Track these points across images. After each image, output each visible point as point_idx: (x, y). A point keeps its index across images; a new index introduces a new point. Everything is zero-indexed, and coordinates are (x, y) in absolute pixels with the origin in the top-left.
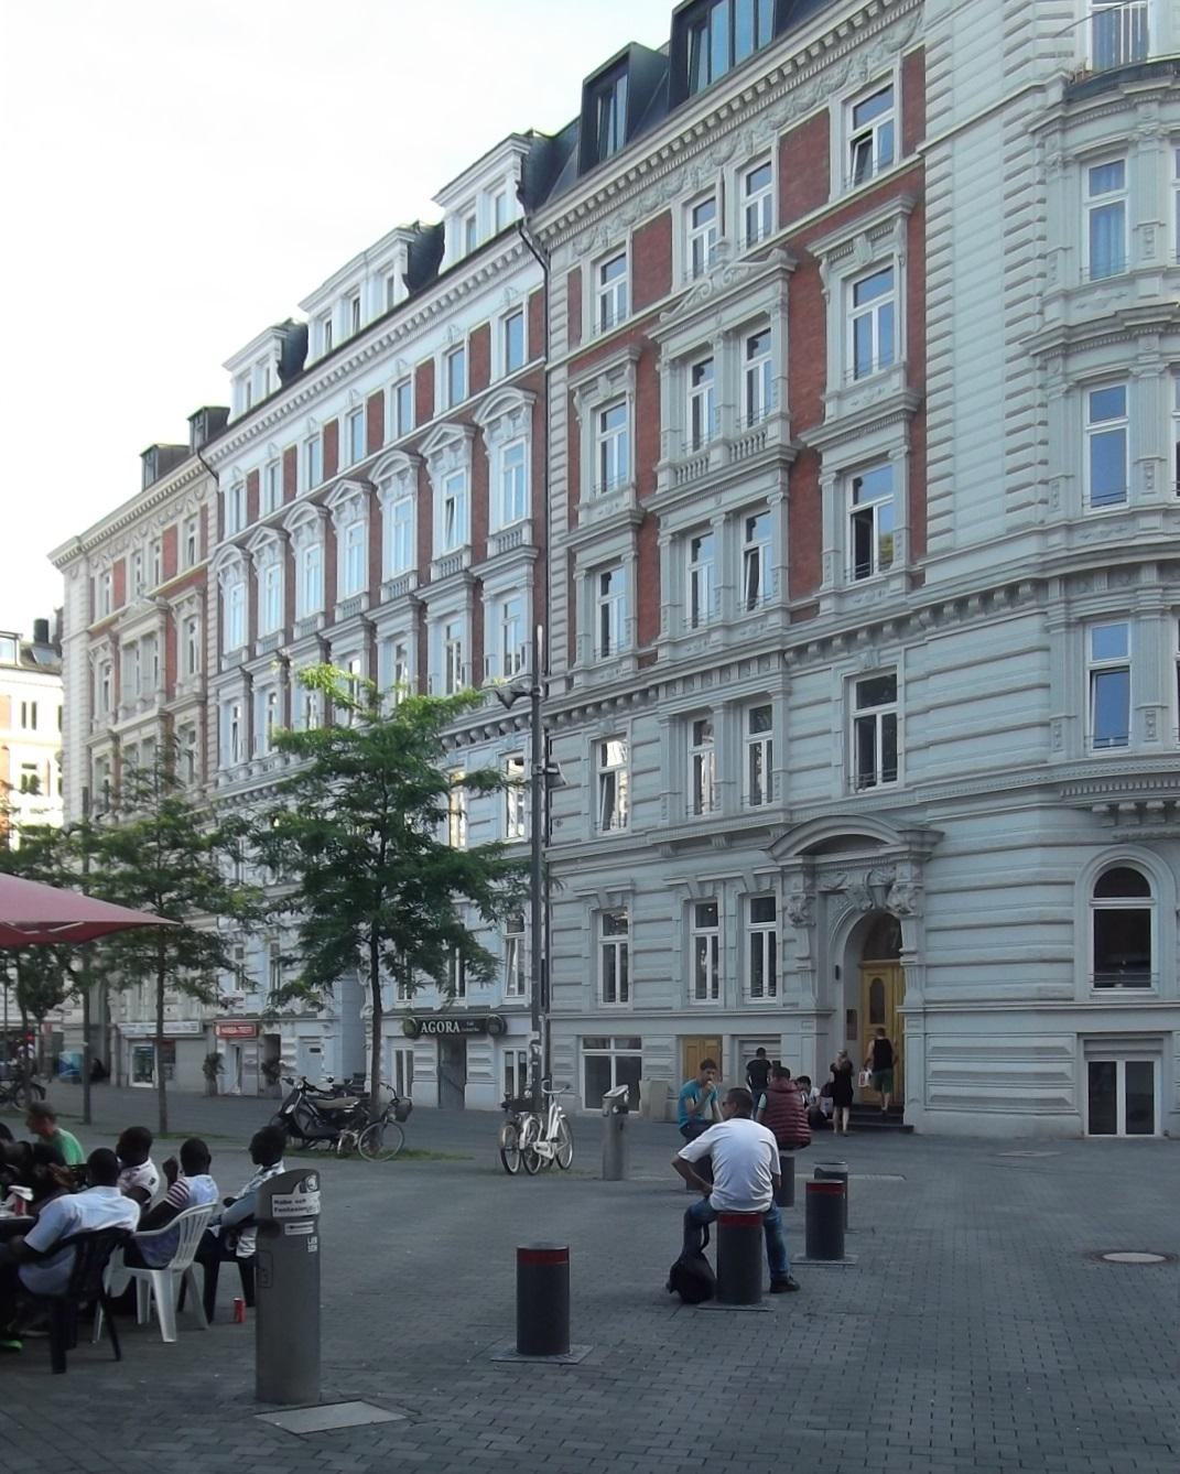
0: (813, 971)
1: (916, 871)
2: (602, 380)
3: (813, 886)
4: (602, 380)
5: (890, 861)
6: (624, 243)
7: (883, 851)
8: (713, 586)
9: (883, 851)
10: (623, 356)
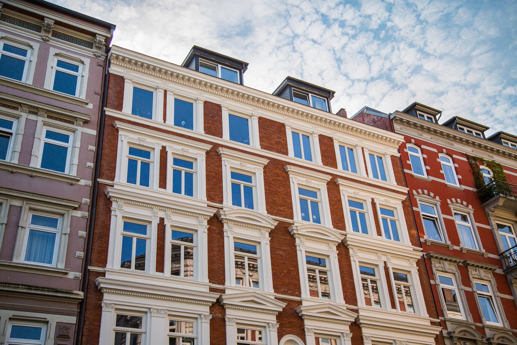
8: (417, 135)
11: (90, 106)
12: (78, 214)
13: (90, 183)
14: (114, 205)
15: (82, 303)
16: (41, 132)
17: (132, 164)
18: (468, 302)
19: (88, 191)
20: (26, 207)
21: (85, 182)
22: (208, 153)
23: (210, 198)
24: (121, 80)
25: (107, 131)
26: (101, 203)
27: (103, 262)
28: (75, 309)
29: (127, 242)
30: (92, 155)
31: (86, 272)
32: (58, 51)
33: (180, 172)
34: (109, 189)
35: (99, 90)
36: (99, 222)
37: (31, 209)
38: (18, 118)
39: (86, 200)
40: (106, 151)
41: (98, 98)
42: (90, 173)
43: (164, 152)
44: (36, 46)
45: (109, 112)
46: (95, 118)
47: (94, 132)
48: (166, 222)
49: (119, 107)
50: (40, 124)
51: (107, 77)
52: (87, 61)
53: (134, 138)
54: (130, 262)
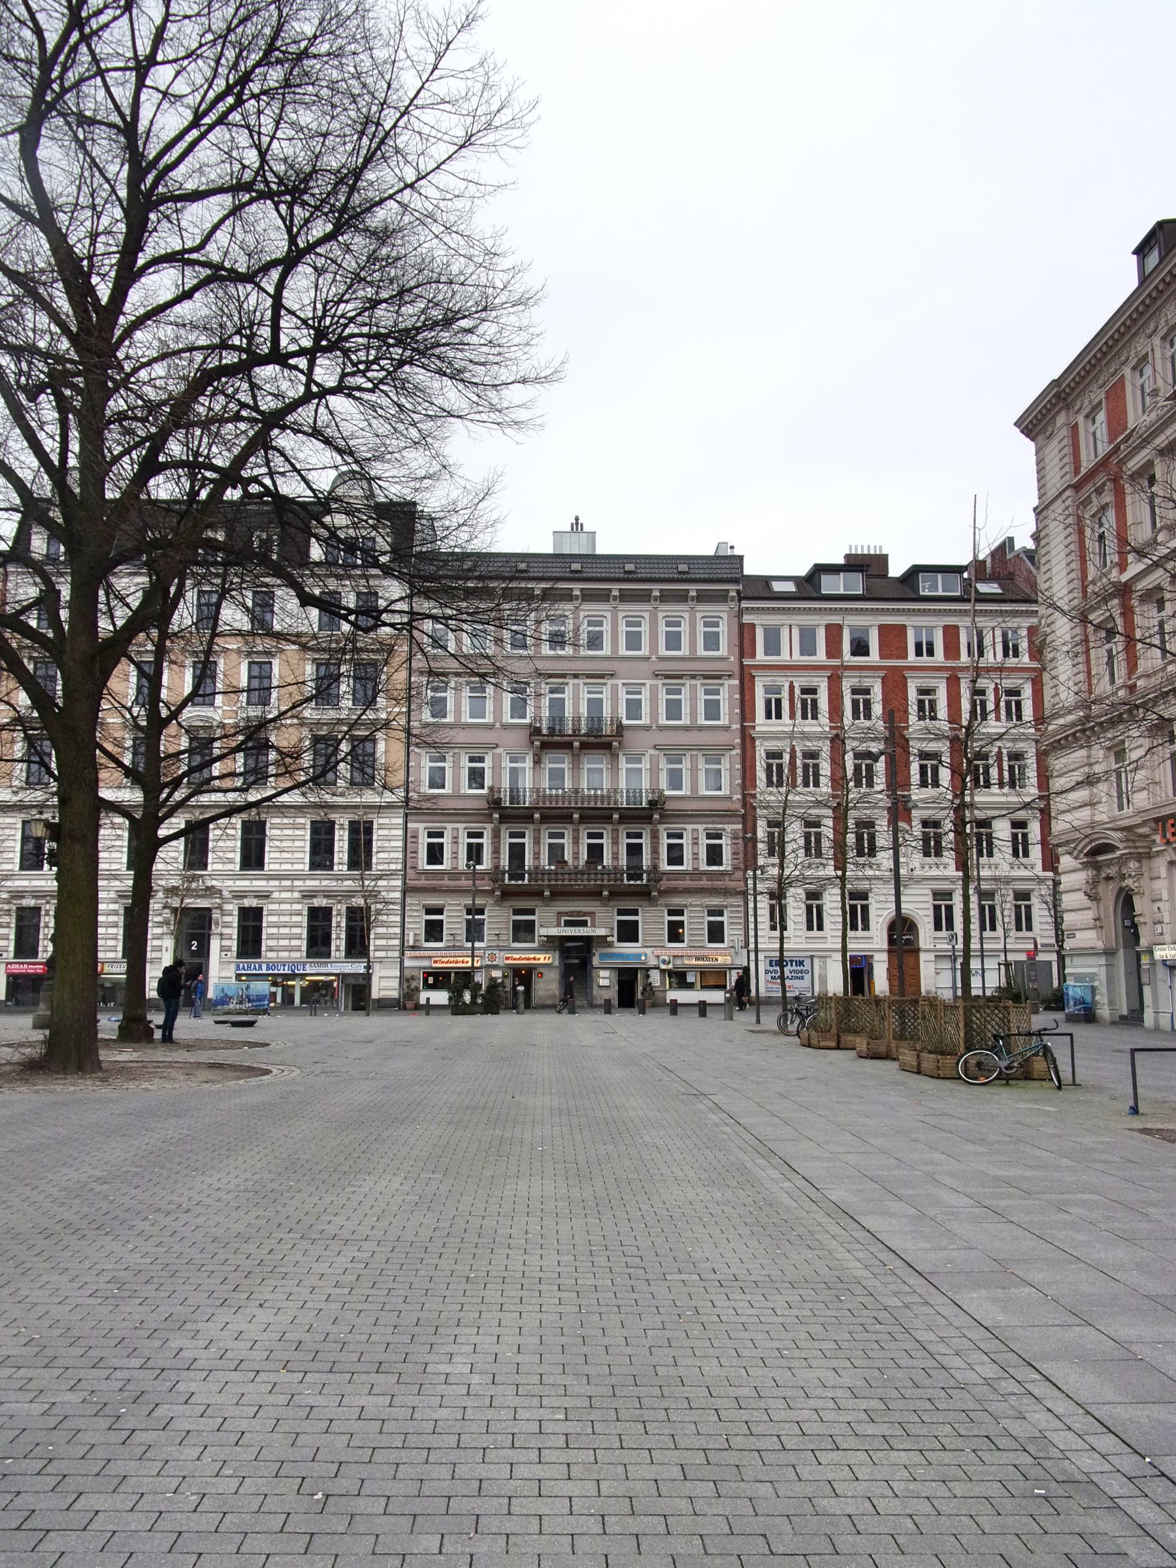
0: (1101, 927)
1: (1137, 865)
2: (1093, 496)
3: (1098, 875)
4: (1093, 496)
5: (1122, 861)
6: (1100, 402)
7: (1118, 853)
9: (1118, 853)
10: (1101, 479)
11: (732, 659)
12: (734, 752)
13: (739, 726)
14: (758, 743)
15: (744, 817)
16: (663, 696)
17: (855, 704)
18: (1174, 782)
19: (738, 734)
20: (700, 754)
21: (736, 726)
22: (883, 678)
23: (831, 720)
24: (753, 626)
25: (746, 679)
26: (748, 741)
27: (755, 786)
28: (740, 820)
29: (769, 768)
30: (738, 702)
31: (744, 796)
32: (587, 613)
33: (858, 700)
34: (752, 732)
35: (737, 643)
36: (748, 757)
37: (664, 684)
38: (722, 685)
39: (738, 741)
40: (747, 698)
41: (737, 649)
42: (738, 718)
43: (792, 687)
44: (686, 615)
45: (747, 662)
46: (736, 669)
47: (737, 682)
48: (797, 749)
49: (753, 655)
50: (620, 686)
51: (741, 626)
52: (724, 616)
53: (854, 682)
54: (439, 768)
